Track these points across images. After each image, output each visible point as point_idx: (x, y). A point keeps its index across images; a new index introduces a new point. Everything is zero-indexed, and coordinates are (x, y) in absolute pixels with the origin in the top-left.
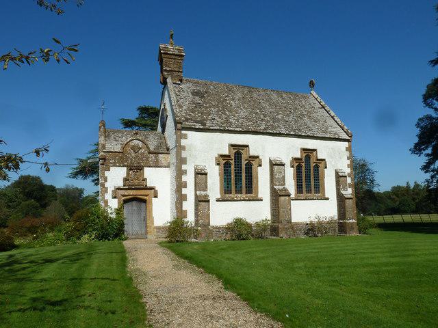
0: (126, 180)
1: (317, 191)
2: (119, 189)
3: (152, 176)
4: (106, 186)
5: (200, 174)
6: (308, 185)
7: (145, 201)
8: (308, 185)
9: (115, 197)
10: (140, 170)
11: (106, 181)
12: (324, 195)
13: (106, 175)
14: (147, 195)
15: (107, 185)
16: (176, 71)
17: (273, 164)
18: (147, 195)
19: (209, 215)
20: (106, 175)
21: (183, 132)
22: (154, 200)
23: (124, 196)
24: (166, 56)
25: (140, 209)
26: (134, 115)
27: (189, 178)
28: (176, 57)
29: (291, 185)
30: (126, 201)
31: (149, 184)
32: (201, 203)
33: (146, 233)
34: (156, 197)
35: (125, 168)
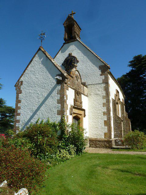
18: (81, 115)
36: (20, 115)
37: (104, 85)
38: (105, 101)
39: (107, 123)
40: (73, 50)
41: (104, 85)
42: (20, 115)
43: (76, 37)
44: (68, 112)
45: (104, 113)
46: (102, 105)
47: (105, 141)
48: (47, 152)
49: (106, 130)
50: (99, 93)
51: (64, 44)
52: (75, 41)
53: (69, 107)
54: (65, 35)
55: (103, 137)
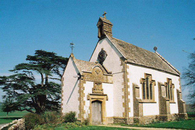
0: (94, 89)
1: (151, 98)
2: (91, 95)
3: (106, 88)
4: (84, 93)
5: (135, 87)
6: (148, 96)
7: (101, 102)
8: (148, 96)
9: (89, 100)
10: (100, 84)
11: (84, 89)
12: (154, 100)
13: (84, 86)
14: (103, 99)
15: (84, 92)
16: (109, 32)
17: (160, 85)
18: (103, 99)
19: (143, 110)
20: (84, 86)
21: (127, 64)
22: (106, 101)
23: (92, 99)
24: (105, 24)
25: (98, 106)
26: (33, 54)
27: (130, 90)
28: (109, 25)
29: (141, 97)
30: (93, 102)
31: (104, 93)
32: (140, 104)
33: (102, 121)
34: (107, 100)
35: (93, 82)
36: (28, 56)
37: (122, 74)
38: (123, 87)
39: (125, 105)
40: (104, 45)
41: (122, 74)
42: (28, 56)
43: (105, 34)
44: (85, 99)
45: (123, 97)
46: (121, 90)
47: (123, 119)
48: (53, 87)
49: (124, 111)
50: (119, 80)
51: (99, 40)
52: (105, 38)
53: (86, 95)
54: (98, 34)
55: (121, 116)
